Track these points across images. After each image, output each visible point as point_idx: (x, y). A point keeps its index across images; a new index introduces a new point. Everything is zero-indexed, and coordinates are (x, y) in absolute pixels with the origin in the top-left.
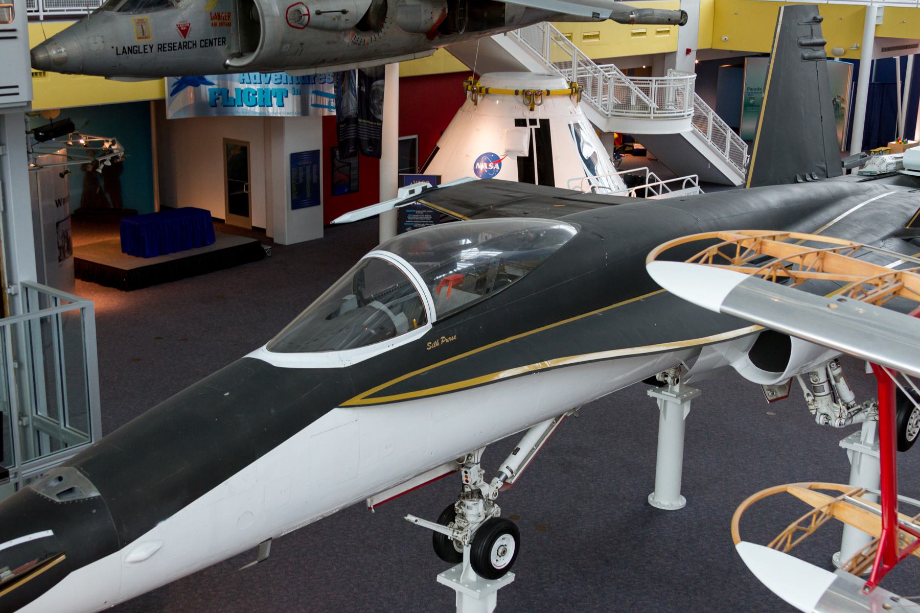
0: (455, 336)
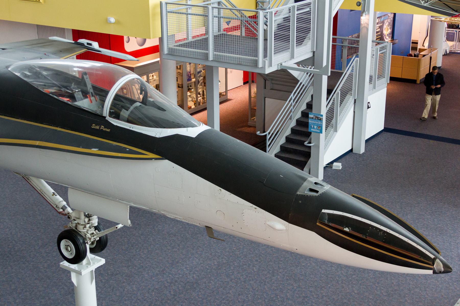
0: (110, 130)
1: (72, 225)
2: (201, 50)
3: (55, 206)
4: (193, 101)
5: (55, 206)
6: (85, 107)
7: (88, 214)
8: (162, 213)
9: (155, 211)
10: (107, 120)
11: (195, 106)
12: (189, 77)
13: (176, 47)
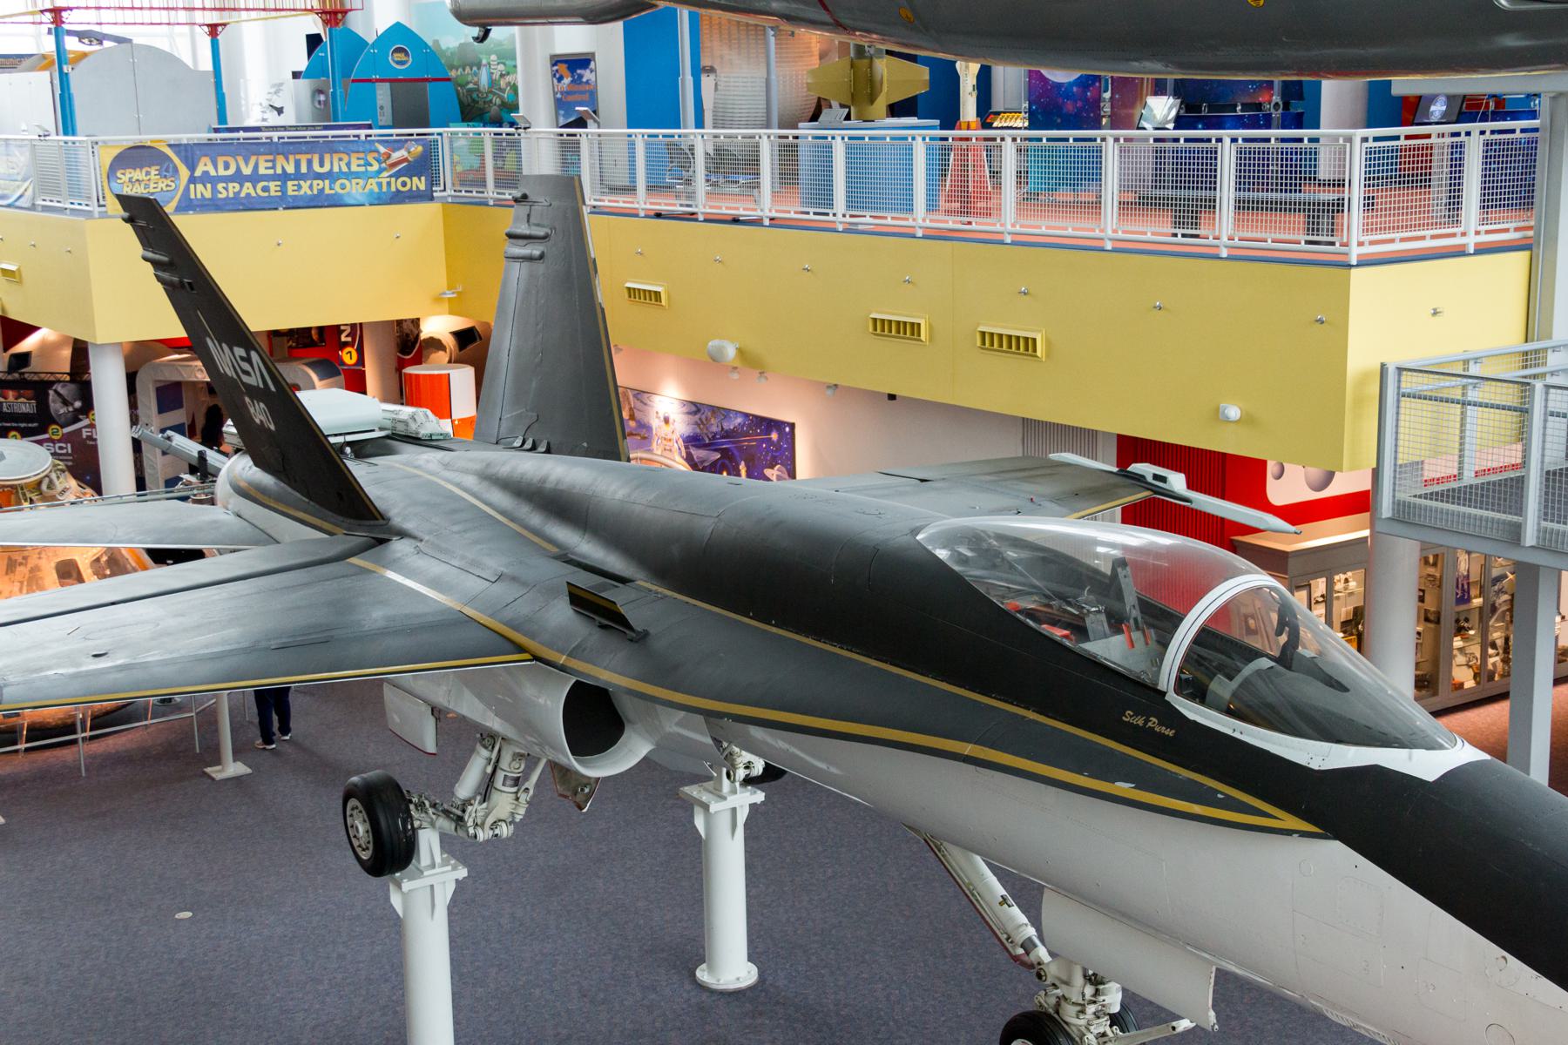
0: (1173, 731)
1: (1047, 1001)
2: (1499, 511)
3: (1004, 937)
4: (1470, 667)
5: (1005, 936)
6: (1113, 659)
7: (1094, 974)
8: (1313, 1005)
9: (1292, 994)
10: (1168, 703)
11: (1478, 683)
12: (1463, 590)
13: (1418, 501)
